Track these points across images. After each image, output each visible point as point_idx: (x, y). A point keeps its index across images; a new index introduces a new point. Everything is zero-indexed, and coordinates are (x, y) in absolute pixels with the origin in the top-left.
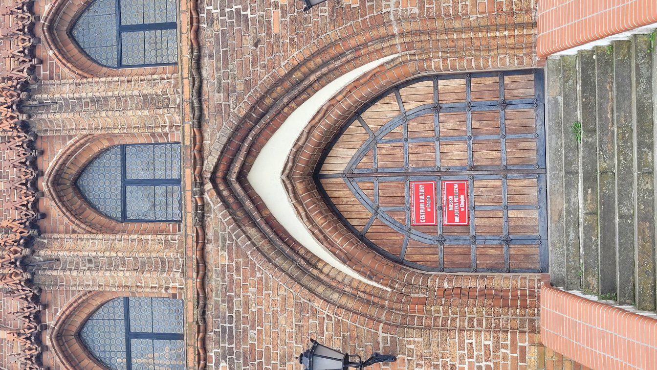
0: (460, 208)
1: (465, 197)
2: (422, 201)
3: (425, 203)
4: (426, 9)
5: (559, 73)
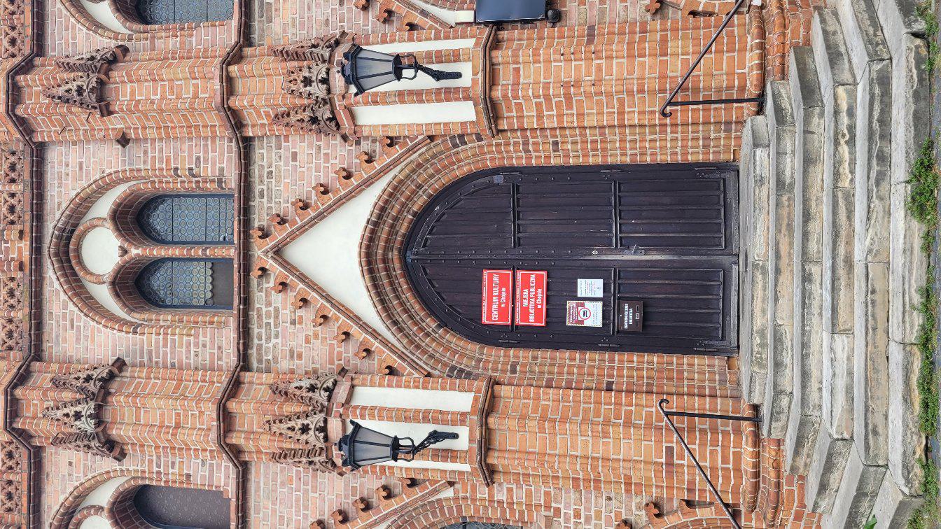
0: (536, 305)
1: (543, 292)
2: (200, 252)
3: (500, 297)
4: (697, 442)
5: (880, 154)
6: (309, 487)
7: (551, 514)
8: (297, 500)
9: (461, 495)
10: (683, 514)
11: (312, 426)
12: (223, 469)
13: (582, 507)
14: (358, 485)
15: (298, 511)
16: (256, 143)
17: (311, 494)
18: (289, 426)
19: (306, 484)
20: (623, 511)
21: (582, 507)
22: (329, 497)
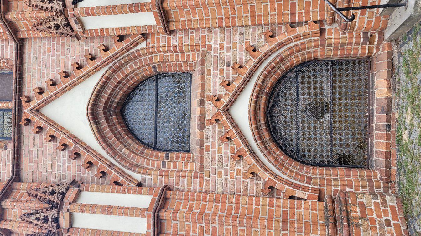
4: (304, 231)
6: (60, 53)
7: (206, 49)
8: (53, 62)
9: (151, 45)
10: (288, 33)
11: (50, 218)
12: (9, 48)
13: (225, 42)
14: (89, 48)
15: (53, 68)
16: (27, 40)
17: (61, 57)
18: (37, 216)
19: (58, 51)
20: (250, 40)
21: (225, 42)
22: (72, 57)
